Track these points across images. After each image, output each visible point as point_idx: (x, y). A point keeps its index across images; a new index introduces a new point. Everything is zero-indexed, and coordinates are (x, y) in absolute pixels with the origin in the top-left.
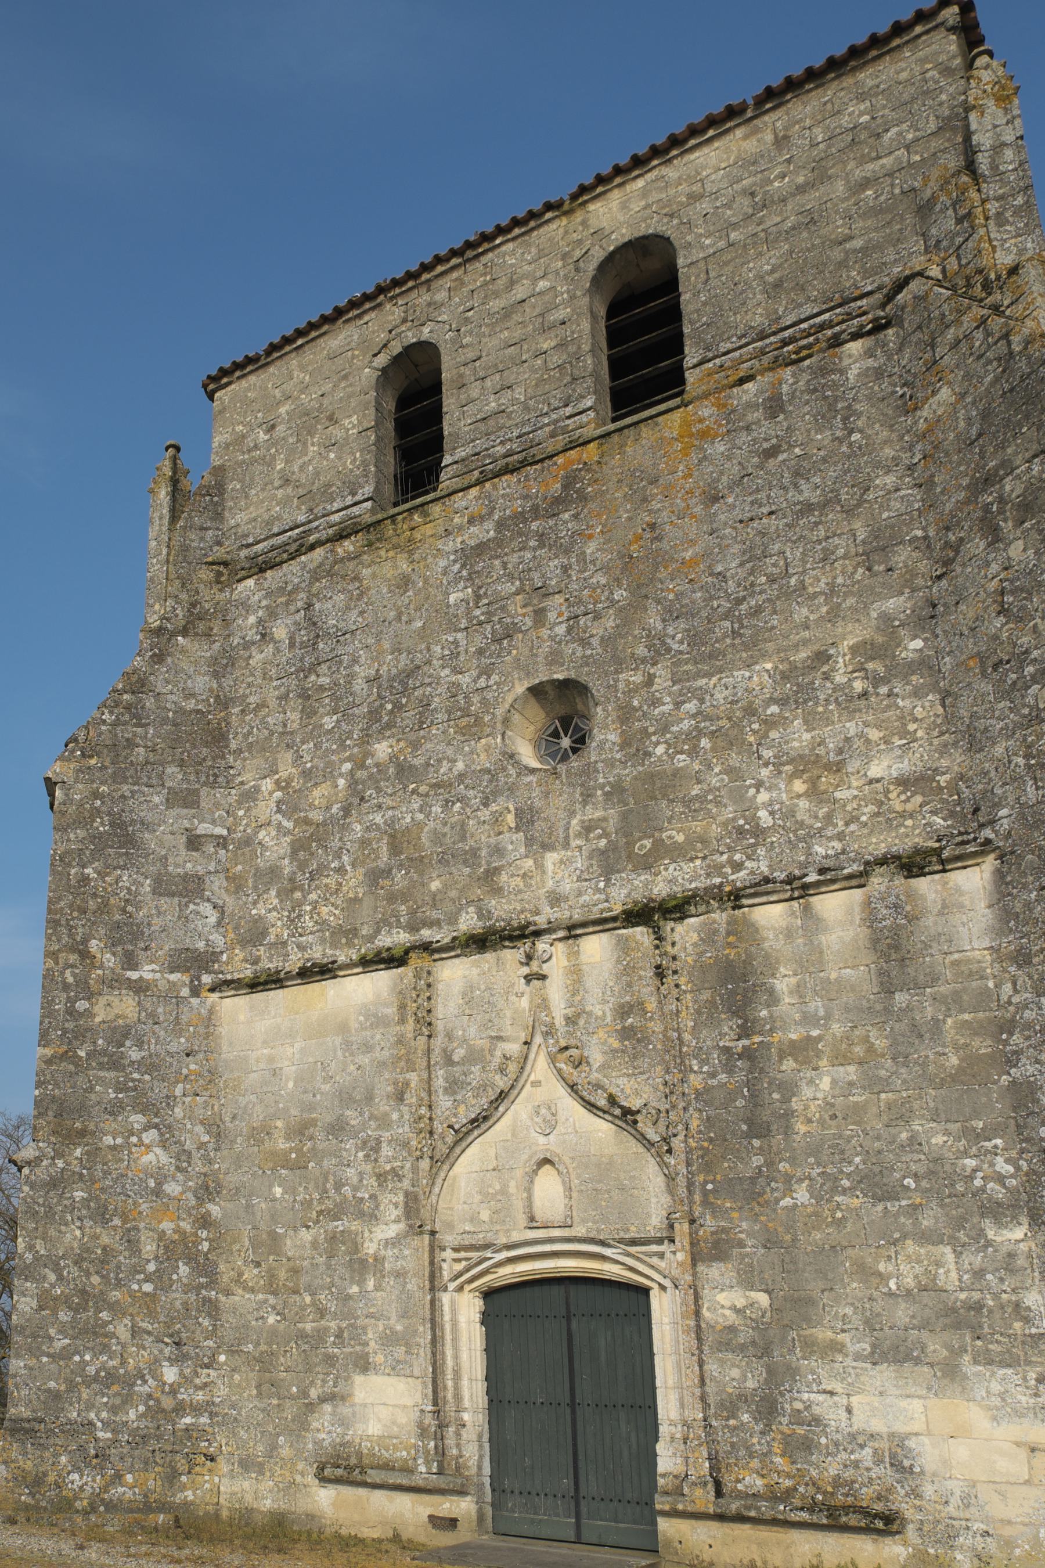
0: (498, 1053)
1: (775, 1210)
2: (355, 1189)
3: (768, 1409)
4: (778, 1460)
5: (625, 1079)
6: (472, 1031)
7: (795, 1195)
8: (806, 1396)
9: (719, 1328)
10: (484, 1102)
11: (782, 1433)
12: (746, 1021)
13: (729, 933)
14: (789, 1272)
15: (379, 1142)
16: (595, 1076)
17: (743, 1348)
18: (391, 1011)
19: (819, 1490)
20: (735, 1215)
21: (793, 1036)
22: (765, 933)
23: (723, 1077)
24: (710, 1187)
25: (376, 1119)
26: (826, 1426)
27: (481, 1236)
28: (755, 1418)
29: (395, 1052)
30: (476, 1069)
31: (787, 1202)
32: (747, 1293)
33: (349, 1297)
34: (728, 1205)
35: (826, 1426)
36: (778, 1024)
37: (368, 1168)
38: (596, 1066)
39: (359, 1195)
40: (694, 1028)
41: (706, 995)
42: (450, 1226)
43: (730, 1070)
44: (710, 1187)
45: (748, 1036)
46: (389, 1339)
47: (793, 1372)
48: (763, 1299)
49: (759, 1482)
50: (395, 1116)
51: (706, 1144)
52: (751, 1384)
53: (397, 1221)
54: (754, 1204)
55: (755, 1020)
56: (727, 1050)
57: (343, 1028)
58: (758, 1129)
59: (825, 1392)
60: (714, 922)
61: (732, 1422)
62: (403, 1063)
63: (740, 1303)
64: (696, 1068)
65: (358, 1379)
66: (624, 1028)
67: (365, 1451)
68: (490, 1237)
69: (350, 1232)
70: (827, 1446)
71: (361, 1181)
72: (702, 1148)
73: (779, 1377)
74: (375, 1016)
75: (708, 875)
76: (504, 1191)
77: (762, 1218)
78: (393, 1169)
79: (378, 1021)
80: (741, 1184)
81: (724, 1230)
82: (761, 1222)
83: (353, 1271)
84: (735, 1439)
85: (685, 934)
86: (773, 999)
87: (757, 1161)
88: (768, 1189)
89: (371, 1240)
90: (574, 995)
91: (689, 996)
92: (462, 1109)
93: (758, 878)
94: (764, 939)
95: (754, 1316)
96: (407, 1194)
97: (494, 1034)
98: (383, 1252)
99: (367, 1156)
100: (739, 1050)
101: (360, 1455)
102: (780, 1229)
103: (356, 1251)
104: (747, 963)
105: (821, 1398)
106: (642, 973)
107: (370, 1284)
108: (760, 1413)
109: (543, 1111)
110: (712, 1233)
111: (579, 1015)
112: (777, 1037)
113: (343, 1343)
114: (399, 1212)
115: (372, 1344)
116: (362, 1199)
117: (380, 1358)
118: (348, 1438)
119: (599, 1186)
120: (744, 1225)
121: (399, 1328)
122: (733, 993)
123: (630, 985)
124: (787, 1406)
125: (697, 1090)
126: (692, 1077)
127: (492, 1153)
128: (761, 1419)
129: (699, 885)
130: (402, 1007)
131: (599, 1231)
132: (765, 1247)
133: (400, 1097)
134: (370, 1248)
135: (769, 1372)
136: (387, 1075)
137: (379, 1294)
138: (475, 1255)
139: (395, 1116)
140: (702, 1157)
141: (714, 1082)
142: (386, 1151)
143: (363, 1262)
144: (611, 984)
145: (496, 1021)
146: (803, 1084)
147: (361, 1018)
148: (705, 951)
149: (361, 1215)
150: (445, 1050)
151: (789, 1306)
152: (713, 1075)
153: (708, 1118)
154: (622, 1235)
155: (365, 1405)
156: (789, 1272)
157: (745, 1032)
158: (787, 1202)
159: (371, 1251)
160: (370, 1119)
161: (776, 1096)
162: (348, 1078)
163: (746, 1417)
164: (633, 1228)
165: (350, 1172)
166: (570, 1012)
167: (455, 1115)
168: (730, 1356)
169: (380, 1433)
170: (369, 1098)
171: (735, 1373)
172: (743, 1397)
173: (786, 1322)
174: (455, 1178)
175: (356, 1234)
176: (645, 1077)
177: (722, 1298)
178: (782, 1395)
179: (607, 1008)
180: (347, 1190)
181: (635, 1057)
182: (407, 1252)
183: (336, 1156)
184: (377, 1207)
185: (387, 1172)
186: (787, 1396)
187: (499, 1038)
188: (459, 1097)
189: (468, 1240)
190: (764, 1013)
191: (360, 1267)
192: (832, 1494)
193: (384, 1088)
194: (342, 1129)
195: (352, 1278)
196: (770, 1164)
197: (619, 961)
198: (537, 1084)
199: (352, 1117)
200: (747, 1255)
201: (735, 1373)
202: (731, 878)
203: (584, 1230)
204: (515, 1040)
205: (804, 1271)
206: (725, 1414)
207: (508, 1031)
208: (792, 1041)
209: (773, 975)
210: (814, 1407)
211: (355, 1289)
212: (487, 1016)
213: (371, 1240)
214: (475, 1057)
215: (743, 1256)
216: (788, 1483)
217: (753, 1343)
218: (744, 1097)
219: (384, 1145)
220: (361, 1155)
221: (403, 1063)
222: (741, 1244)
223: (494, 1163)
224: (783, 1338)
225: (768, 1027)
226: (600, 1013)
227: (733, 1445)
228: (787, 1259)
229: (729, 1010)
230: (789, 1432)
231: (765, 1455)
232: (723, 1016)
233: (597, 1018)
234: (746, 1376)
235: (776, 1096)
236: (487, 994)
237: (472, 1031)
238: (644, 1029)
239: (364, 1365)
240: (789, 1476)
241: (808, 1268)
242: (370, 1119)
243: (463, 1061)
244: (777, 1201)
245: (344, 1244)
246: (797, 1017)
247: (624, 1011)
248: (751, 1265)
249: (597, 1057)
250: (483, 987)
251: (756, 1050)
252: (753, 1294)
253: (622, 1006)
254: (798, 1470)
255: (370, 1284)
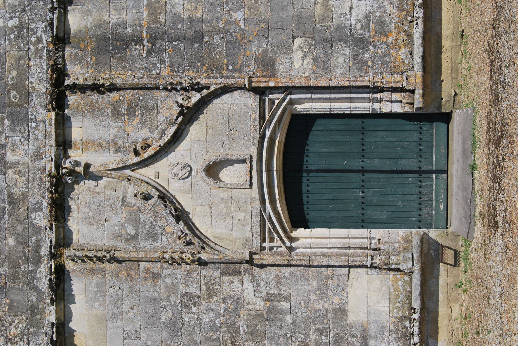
0: (133, 200)
1: (246, 31)
2: (218, 315)
3: (361, 43)
4: (390, 39)
5: (160, 115)
6: (116, 219)
7: (238, 20)
8: (353, 22)
9: (314, 68)
10: (165, 212)
11: (375, 36)
12: (133, 40)
13: (79, 48)
14: (282, 26)
15: (186, 294)
16: (156, 135)
17: (326, 54)
18: (94, 281)
19: (405, 19)
20: (248, 54)
21: (146, 14)
22: (82, 27)
23: (165, 55)
24: (230, 67)
25: (169, 295)
26: (369, 12)
27: (254, 219)
28: (367, 50)
29: (124, 278)
30: (142, 217)
31: (242, 24)
32: (294, 50)
33: (294, 323)
34: (242, 57)
35: (369, 12)
36: (137, 22)
37: (204, 304)
38: (150, 134)
39: (222, 312)
40: (133, 71)
41: (114, 62)
42: (247, 241)
43: (162, 51)
44: (230, 67)
45: (143, 40)
46: (323, 292)
47: (340, 28)
48: (298, 42)
49: (403, 50)
50: (169, 281)
51: (205, 68)
52: (347, 51)
53: (242, 282)
54: (242, 42)
55: (133, 35)
56: (149, 52)
57: (102, 320)
58: (198, 38)
59: (350, 11)
60: (70, 55)
61: (370, 64)
62: (132, 273)
63: (300, 54)
64: (158, 71)
65: (351, 317)
66: (127, 114)
67: (400, 314)
68: (256, 212)
69: (248, 320)
70: (380, 12)
71: (212, 310)
72: (207, 70)
73: (343, 36)
74: (96, 293)
75: (41, 58)
76: (225, 201)
77: (251, 38)
78: (206, 284)
79: (101, 291)
80: (230, 49)
81: (257, 60)
82: (253, 39)
83: (275, 319)
84: (380, 63)
85: (76, 73)
86: (123, 24)
87: (217, 39)
88: (234, 34)
89: (254, 303)
90: (102, 147)
91: (113, 73)
92: (168, 229)
93: (49, 28)
94: (86, 27)
95: (308, 47)
96: (223, 274)
97: (120, 203)
98: (263, 294)
99: (195, 304)
100: (150, 45)
101: (403, 318)
102: (257, 29)
103: (261, 315)
104: (98, 38)
105: (354, 14)
106: (94, 101)
107: (285, 305)
108: (364, 48)
109: (175, 170)
110: (258, 67)
111: (116, 144)
112: (144, 23)
113: (325, 329)
114: (235, 279)
115: (326, 305)
116: (225, 309)
117: (336, 300)
118: (392, 328)
119: (226, 137)
120: (254, 49)
121: (315, 284)
122: (115, 47)
123: (100, 109)
124: (359, 32)
125: (171, 71)
126: (163, 74)
127: (199, 208)
128: (367, 47)
129: (45, 64)
130: (93, 271)
131: (254, 137)
132: (267, 38)
133: (156, 276)
134: (260, 304)
135: (340, 41)
136: (139, 286)
137: (292, 299)
138: (268, 224)
139: (169, 281)
140: (212, 71)
141: (167, 61)
142: (192, 289)
143: (270, 310)
144: (98, 121)
145: (112, 202)
146: (175, 11)
147: (96, 304)
148: (87, 61)
149: (236, 310)
150: (127, 240)
151: (302, 27)
152: (163, 61)
153: (189, 66)
154: (257, 123)
155: (369, 313)
156: (282, 26)
157: (139, 41)
158: (242, 24)
159: (262, 304)
160: (169, 301)
161: (180, 26)
162: (139, 317)
163: (367, 56)
164: (253, 116)
165: (206, 318)
166: (112, 149)
167: (172, 234)
168: (331, 62)
169: (387, 301)
170: (154, 300)
171: (341, 60)
172: (355, 57)
173: (311, 29)
174: (215, 237)
175: (250, 315)
176: (160, 103)
177: (297, 64)
178: (353, 34)
179: (113, 124)
180: (219, 321)
181: (146, 108)
182: (264, 276)
183: (194, 330)
184: (231, 297)
185: (208, 289)
186: (353, 32)
187: (124, 199)
188: (160, 231)
189: (257, 229)
190: (130, 30)
191: (272, 314)
192: (407, 12)
193: (148, 288)
194: (174, 323)
195: (281, 320)
196: (219, 32)
197: (85, 116)
198: (158, 175)
199: (166, 315)
200: (272, 49)
201: (341, 60)
202: (45, 44)
203: (254, 147)
204: (126, 189)
205: (282, 17)
206: (365, 67)
207: (119, 193)
208: (149, 15)
209: (108, 23)
210: (359, 18)
211: (288, 317)
212: (108, 208)
213: (254, 303)
214: (134, 220)
215: (272, 51)
216: (403, 34)
217: (323, 48)
218: (178, 44)
219: (188, 291)
220: (194, 309)
221: (132, 273)
222: (266, 51)
223: (207, 207)
224: (321, 31)
225: (138, 28)
226: (116, 129)
227: (383, 64)
228: (275, 26)
229: (125, 49)
230: (374, 33)
231: (388, 46)
232: (128, 53)
233: (119, 132)
234: (343, 54)
235: (180, 26)
236: (93, 207)
237: (116, 219)
238: (130, 102)
239: (341, 312)
240: (399, 33)
241: (281, 15)
242: (169, 301)
243: (136, 227)
244: (241, 29)
245: (256, 325)
246: (134, 11)
247: (117, 114)
248: (278, 47)
249: (144, 133)
250: (87, 210)
251: (151, 36)
252: (295, 47)
253: (113, 115)
254: (395, 28)
255: (285, 305)
